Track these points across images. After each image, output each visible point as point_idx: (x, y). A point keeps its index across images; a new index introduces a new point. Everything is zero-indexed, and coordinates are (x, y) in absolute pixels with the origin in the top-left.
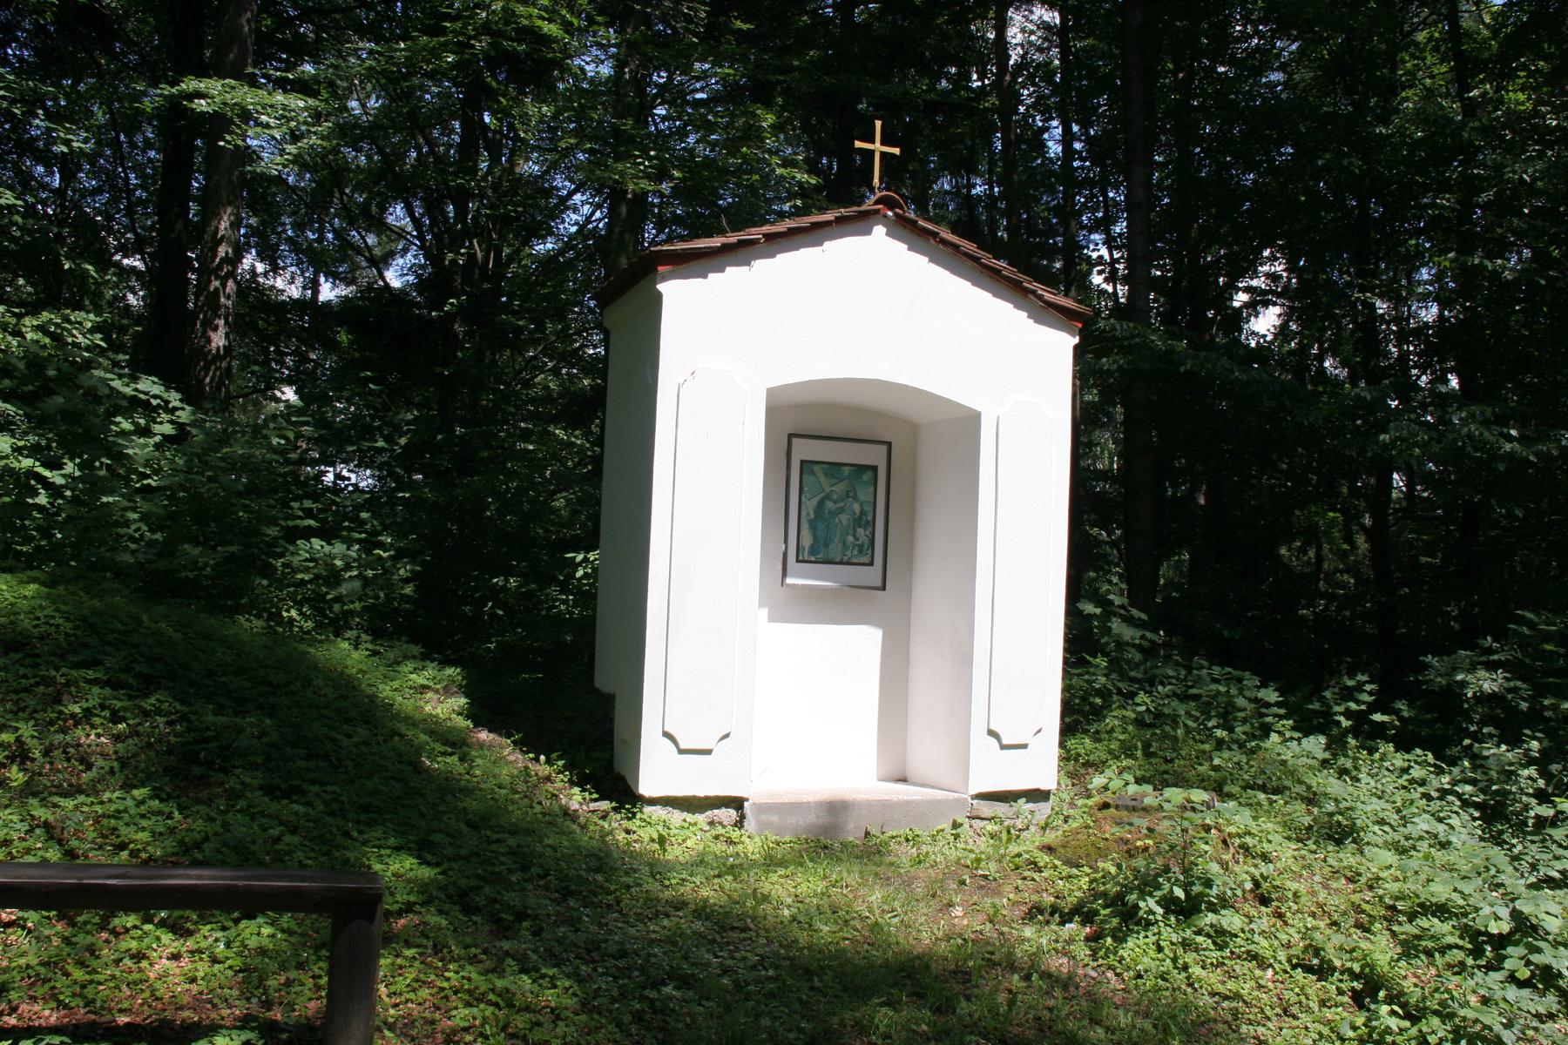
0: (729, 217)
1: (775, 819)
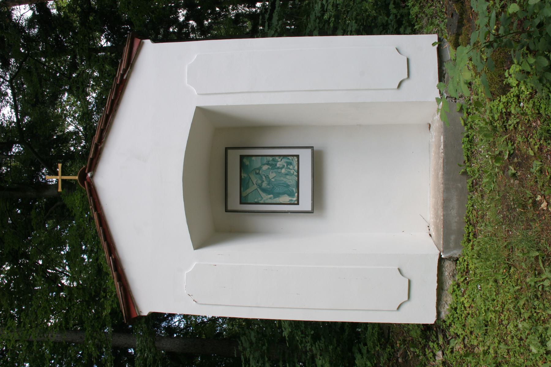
0: (106, 273)
1: (453, 237)
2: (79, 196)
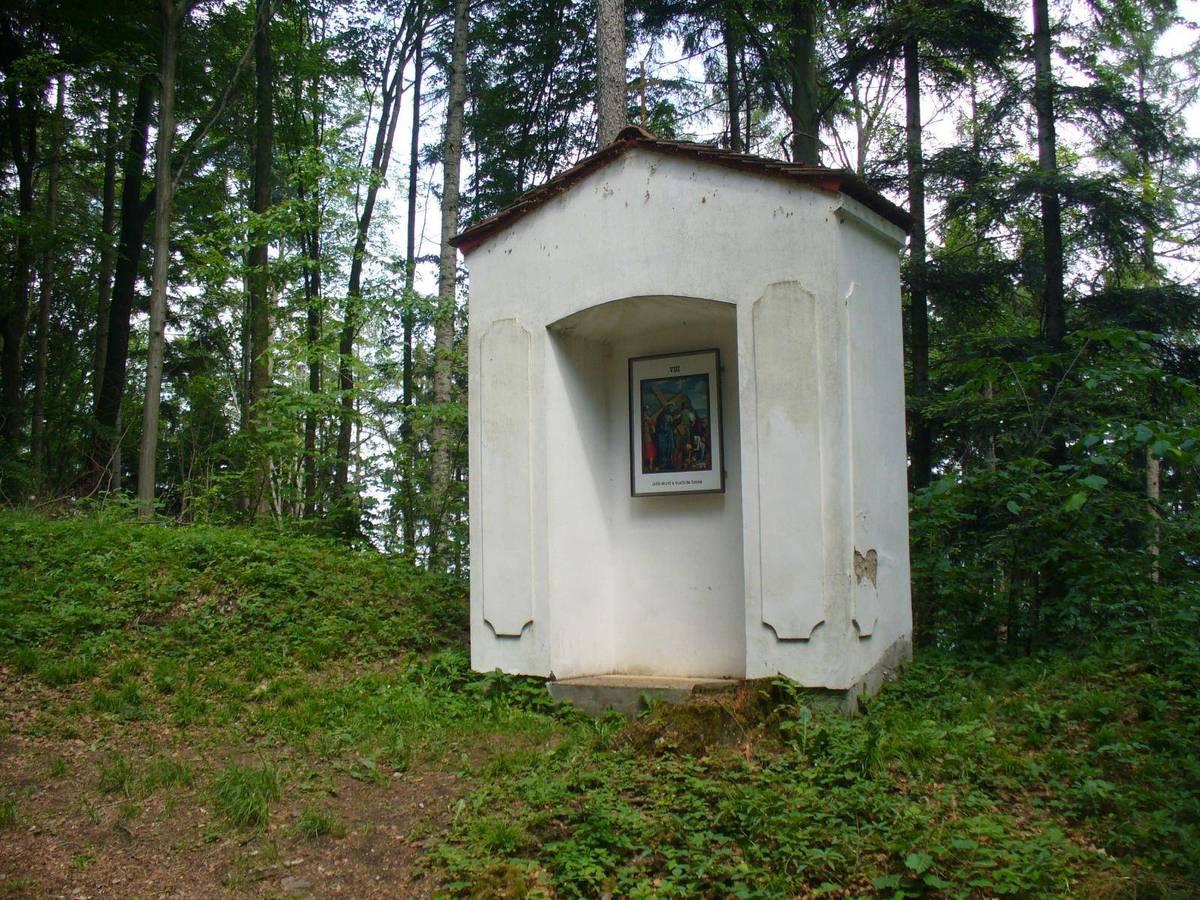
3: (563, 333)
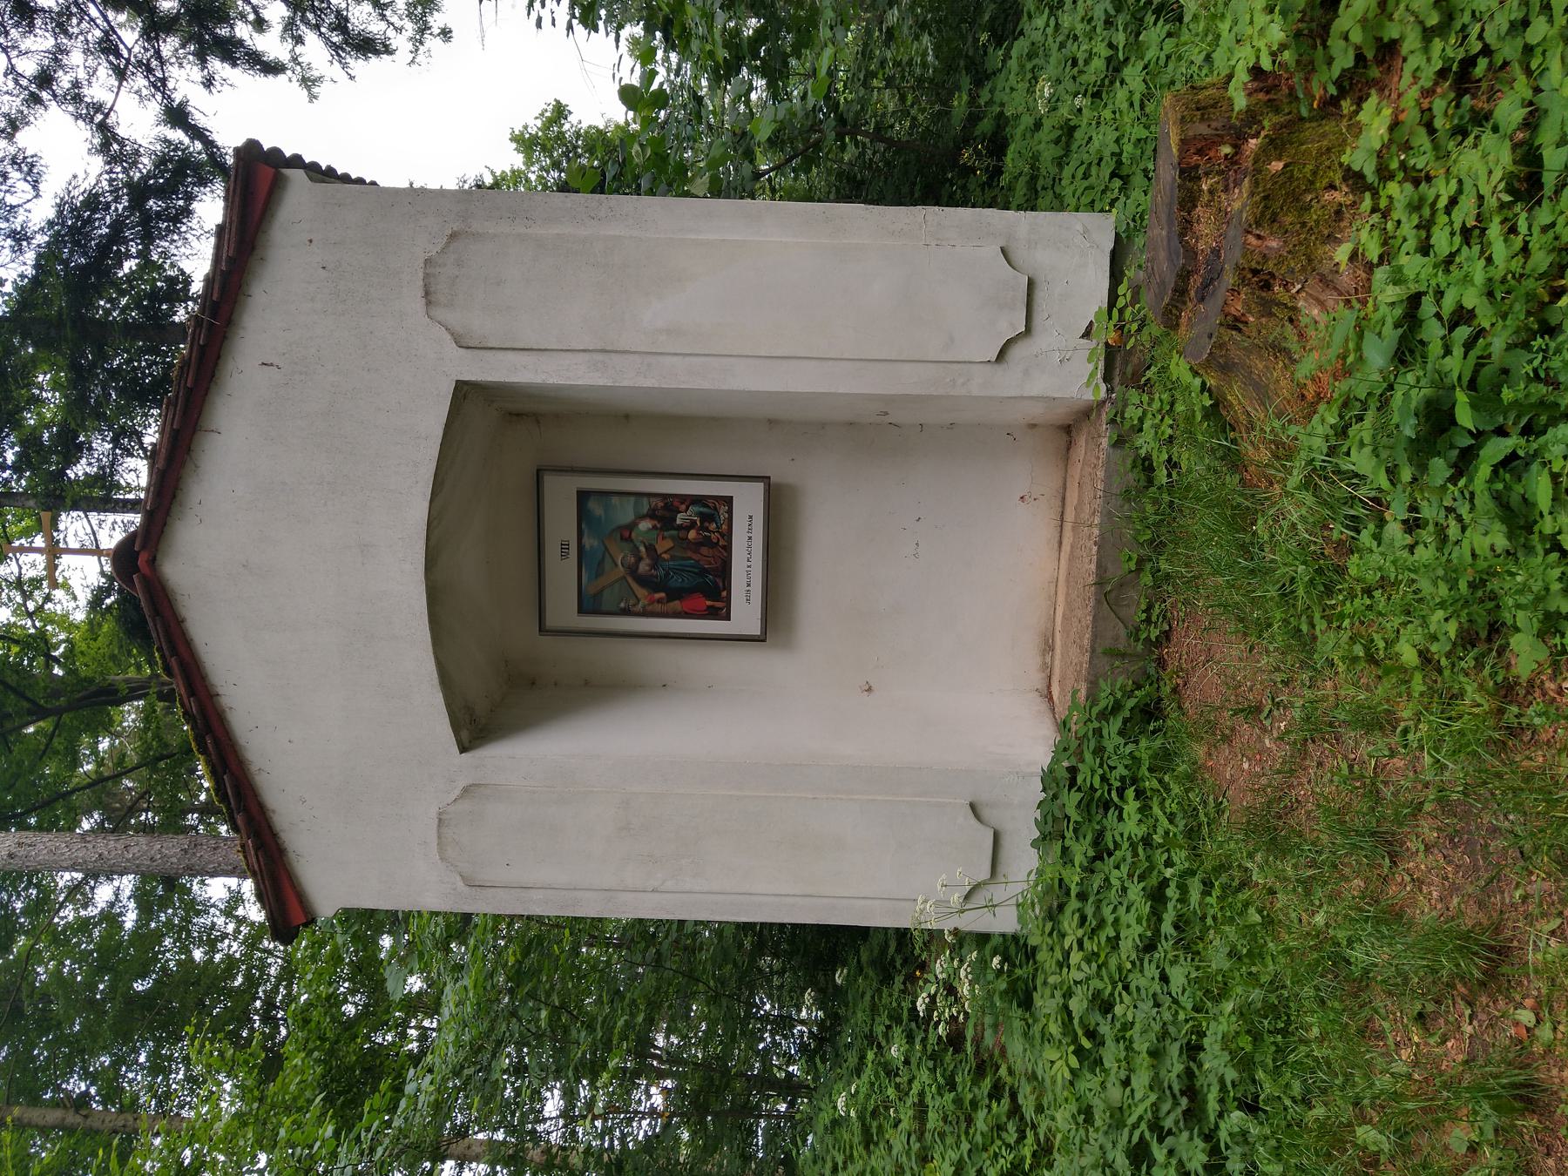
2: (1392, 890)
3: (475, 726)
